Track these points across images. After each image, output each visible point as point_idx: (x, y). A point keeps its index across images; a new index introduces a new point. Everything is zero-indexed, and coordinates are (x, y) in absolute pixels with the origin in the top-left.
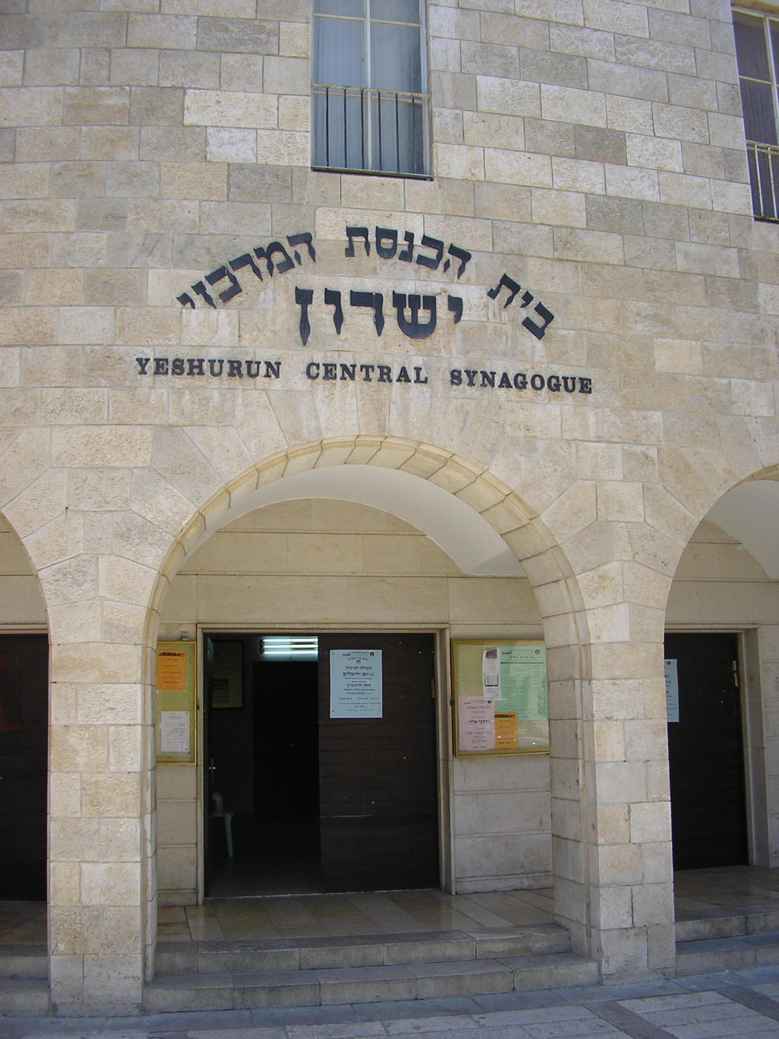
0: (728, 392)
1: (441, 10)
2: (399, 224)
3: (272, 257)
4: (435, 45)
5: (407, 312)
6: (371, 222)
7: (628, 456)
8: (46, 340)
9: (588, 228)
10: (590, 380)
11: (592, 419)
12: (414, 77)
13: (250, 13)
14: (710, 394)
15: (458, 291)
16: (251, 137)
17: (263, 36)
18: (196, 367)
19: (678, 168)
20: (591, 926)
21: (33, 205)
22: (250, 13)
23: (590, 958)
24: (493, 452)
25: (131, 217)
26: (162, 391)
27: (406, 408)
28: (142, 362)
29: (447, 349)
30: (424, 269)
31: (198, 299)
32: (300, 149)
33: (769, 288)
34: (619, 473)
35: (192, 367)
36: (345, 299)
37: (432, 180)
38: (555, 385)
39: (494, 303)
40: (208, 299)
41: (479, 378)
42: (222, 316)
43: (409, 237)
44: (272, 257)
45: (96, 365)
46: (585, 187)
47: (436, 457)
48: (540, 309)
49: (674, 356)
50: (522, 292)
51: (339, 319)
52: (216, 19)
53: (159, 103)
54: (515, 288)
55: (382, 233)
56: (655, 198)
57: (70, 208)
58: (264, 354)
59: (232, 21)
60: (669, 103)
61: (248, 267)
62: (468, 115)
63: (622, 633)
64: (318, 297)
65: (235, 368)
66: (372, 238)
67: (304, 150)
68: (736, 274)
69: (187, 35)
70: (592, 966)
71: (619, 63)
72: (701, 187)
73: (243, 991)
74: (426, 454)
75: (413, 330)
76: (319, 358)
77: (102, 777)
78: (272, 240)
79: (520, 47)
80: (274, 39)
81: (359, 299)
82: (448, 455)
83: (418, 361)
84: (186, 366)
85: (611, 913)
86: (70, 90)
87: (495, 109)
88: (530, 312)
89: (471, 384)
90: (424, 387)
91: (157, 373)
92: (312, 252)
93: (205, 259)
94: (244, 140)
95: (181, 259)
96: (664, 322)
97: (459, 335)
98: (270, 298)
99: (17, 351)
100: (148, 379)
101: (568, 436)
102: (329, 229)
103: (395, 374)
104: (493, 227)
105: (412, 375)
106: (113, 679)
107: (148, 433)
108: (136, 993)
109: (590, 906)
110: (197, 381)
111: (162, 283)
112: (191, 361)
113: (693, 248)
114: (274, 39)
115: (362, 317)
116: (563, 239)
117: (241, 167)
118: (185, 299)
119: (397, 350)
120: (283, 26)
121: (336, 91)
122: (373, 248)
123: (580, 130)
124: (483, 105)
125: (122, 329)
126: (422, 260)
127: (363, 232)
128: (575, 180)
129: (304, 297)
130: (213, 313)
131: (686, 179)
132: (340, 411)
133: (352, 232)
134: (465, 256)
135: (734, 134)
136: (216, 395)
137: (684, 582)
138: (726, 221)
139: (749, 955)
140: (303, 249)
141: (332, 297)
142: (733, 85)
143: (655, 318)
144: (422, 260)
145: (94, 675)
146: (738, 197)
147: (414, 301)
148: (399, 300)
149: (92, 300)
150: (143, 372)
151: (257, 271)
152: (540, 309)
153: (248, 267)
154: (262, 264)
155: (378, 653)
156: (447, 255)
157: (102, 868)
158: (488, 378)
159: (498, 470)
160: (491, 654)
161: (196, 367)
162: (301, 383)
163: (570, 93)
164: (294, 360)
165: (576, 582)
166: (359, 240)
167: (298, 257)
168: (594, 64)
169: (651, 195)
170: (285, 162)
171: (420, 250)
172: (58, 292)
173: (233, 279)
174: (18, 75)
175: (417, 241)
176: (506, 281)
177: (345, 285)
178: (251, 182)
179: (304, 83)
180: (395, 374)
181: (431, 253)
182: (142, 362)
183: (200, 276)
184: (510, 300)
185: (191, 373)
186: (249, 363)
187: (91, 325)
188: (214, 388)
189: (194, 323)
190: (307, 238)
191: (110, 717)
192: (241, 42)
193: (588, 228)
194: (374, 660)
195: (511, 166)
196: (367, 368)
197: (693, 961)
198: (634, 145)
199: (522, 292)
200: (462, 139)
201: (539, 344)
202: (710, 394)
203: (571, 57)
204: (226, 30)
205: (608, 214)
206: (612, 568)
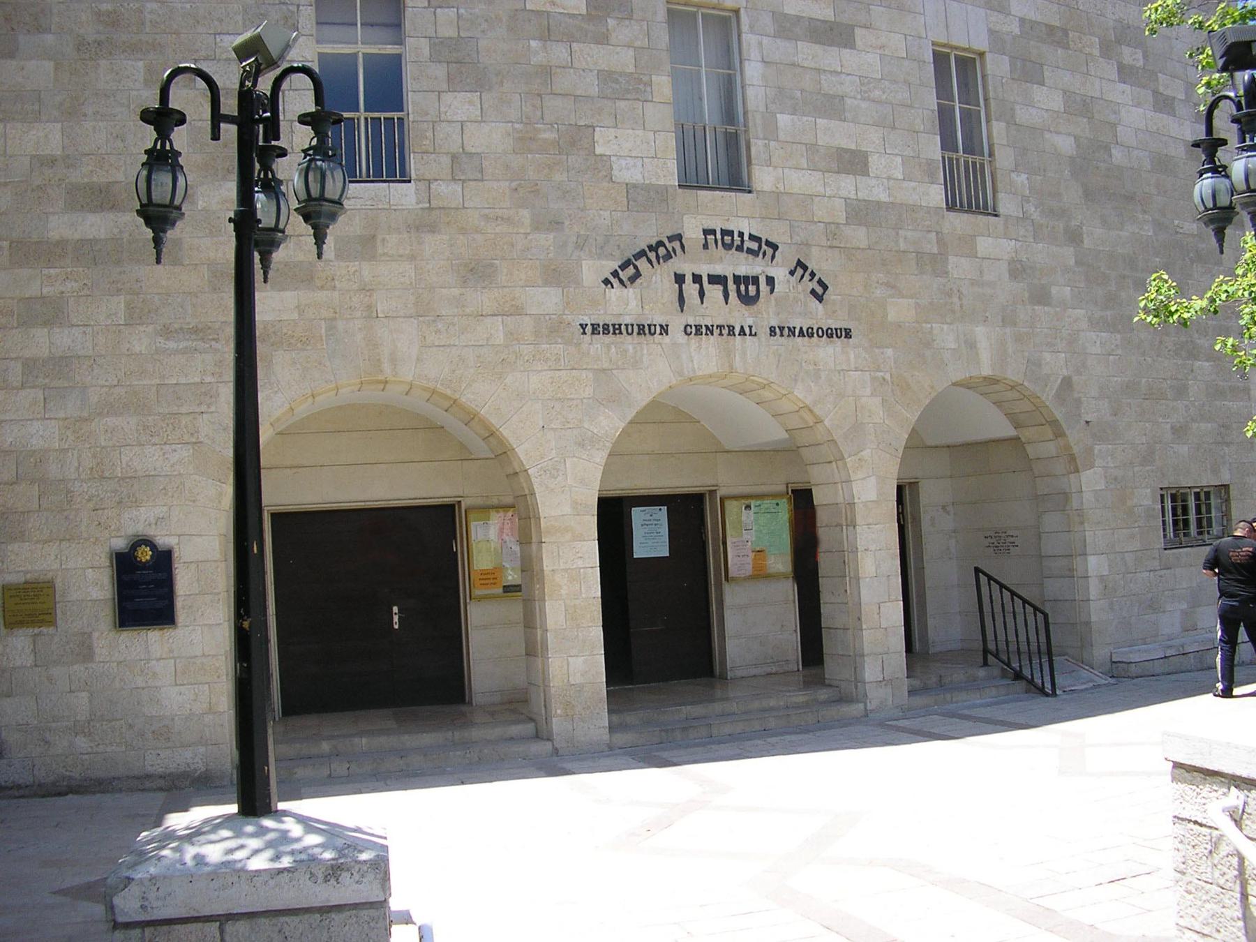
0: (931, 333)
1: (753, 64)
2: (733, 226)
3: (659, 251)
4: (750, 92)
5: (743, 288)
6: (718, 225)
7: (874, 379)
8: (518, 311)
9: (847, 224)
11: (852, 356)
12: (729, 111)
13: (631, 69)
14: (920, 335)
15: (772, 272)
16: (639, 164)
17: (641, 86)
18: (617, 329)
19: (901, 177)
20: (859, 681)
21: (500, 213)
22: (631, 69)
23: (858, 701)
24: (796, 381)
25: (567, 223)
27: (744, 353)
28: (583, 326)
29: (767, 313)
30: (751, 257)
31: (615, 282)
32: (669, 174)
33: (955, 259)
34: (868, 391)
35: (615, 329)
36: (705, 279)
37: (750, 192)
38: (830, 333)
39: (793, 279)
40: (621, 281)
41: (786, 331)
42: (631, 293)
43: (741, 234)
44: (659, 251)
45: (553, 328)
46: (844, 193)
47: (758, 384)
48: (820, 282)
49: (899, 310)
50: (809, 271)
51: (702, 294)
52: (610, 73)
53: (577, 139)
54: (805, 268)
55: (725, 232)
56: (887, 200)
57: (525, 215)
58: (659, 320)
59: (621, 74)
60: (894, 128)
61: (644, 259)
62: (772, 143)
63: (873, 496)
64: (689, 279)
65: (641, 330)
66: (719, 236)
67: (673, 174)
68: (935, 250)
69: (591, 86)
70: (861, 706)
71: (863, 99)
72: (914, 189)
73: (667, 731)
74: (753, 381)
75: (748, 300)
76: (691, 322)
77: (577, 602)
78: (657, 239)
79: (802, 91)
80: (648, 89)
81: (714, 279)
82: (784, 392)
83: (750, 321)
84: (611, 328)
85: (871, 672)
86: (516, 126)
87: (789, 139)
88: (814, 285)
89: (782, 335)
90: (754, 339)
91: (593, 333)
92: (683, 247)
93: (617, 253)
94: (635, 166)
95: (602, 253)
96: (893, 287)
97: (773, 301)
98: (658, 279)
99: (500, 318)
100: (588, 337)
101: (838, 368)
102: (693, 233)
103: (737, 331)
104: (791, 226)
105: (747, 331)
106: (580, 538)
107: (591, 375)
108: (606, 737)
109: (857, 668)
110: (618, 338)
111: (593, 270)
112: (614, 325)
113: (909, 234)
114: (648, 89)
115: (714, 292)
116: (832, 231)
117: (635, 186)
118: (607, 282)
119: (738, 315)
120: (654, 78)
121: (688, 126)
122: (720, 243)
123: (841, 151)
124: (782, 136)
125: (568, 303)
126: (749, 251)
127: (713, 232)
128: (838, 189)
129: (680, 279)
130: (626, 290)
131: (905, 184)
132: (704, 357)
133: (707, 232)
134: (775, 247)
135: (933, 149)
136: (630, 347)
138: (929, 212)
139: (948, 696)
140: (677, 244)
141: (697, 279)
142: (933, 111)
143: (888, 285)
144: (749, 251)
145: (568, 536)
146: (936, 195)
147: (746, 278)
148: (737, 279)
149: (547, 283)
150: (584, 333)
151: (650, 261)
152: (820, 282)
153: (644, 259)
154: (652, 255)
155: (665, 508)
156: (764, 247)
157: (581, 659)
158: (792, 331)
159: (799, 392)
160: (748, 507)
161: (617, 329)
162: (682, 338)
163: (834, 124)
164: (677, 323)
165: (845, 464)
166: (710, 237)
167: (674, 250)
168: (848, 101)
169: (884, 197)
170: (661, 182)
171: (749, 244)
172: (523, 277)
173: (636, 267)
174: (478, 113)
175: (746, 237)
176: (800, 264)
177: (704, 270)
178: (641, 197)
179: (670, 124)
180: (737, 331)
181: (754, 246)
182: (583, 326)
183: (615, 265)
184: (802, 277)
185: (614, 333)
186: (649, 326)
187: (546, 300)
188: (629, 343)
189: (614, 299)
190: (679, 237)
191: (580, 563)
192: (628, 91)
193: (847, 224)
194: (662, 513)
195: (801, 181)
196: (720, 327)
197: (919, 701)
198: (875, 162)
199: (809, 271)
200: (769, 163)
201: (820, 306)
202: (920, 335)
203: (834, 97)
204: (616, 81)
205: (861, 212)
206: (866, 454)
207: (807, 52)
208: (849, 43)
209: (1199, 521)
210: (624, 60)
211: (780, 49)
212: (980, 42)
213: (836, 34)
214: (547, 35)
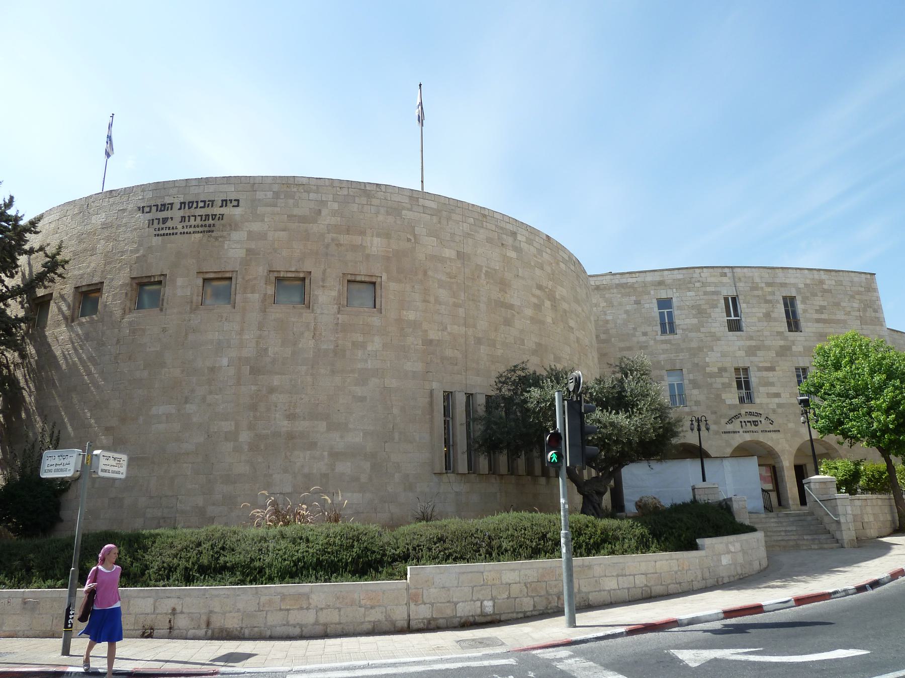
10: (77, 288)
26: (724, 436)
29: (760, 427)
65: (734, 432)
85: (791, 502)
98: (737, 422)
102: (743, 412)
109: (788, 501)
111: (724, 421)
115: (748, 424)
116: (774, 411)
119: (754, 428)
137: (796, 456)
164: (741, 431)
178: (731, 407)
205: (780, 406)
207: (765, 374)
208: (775, 370)
209: (789, 531)
210: (727, 380)
211: (759, 374)
212: (807, 365)
213: (771, 369)
214: (711, 377)
